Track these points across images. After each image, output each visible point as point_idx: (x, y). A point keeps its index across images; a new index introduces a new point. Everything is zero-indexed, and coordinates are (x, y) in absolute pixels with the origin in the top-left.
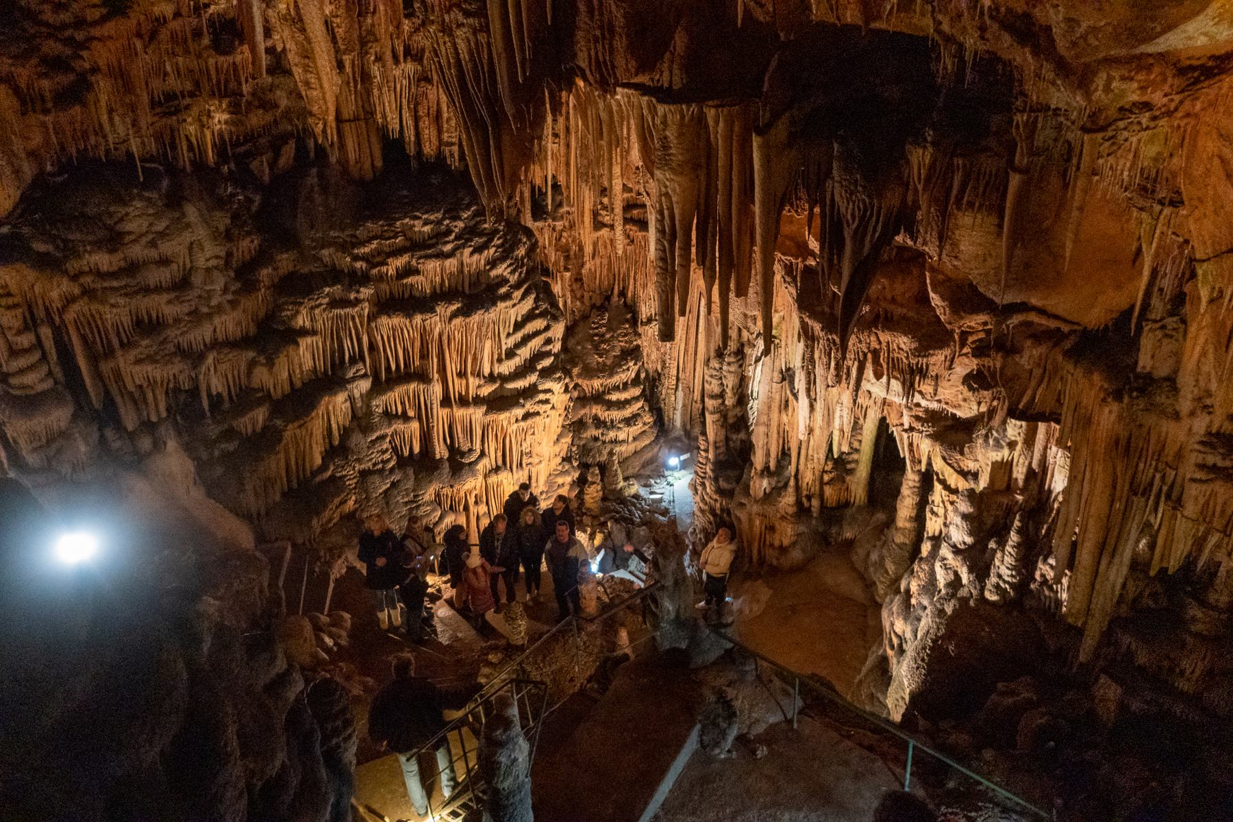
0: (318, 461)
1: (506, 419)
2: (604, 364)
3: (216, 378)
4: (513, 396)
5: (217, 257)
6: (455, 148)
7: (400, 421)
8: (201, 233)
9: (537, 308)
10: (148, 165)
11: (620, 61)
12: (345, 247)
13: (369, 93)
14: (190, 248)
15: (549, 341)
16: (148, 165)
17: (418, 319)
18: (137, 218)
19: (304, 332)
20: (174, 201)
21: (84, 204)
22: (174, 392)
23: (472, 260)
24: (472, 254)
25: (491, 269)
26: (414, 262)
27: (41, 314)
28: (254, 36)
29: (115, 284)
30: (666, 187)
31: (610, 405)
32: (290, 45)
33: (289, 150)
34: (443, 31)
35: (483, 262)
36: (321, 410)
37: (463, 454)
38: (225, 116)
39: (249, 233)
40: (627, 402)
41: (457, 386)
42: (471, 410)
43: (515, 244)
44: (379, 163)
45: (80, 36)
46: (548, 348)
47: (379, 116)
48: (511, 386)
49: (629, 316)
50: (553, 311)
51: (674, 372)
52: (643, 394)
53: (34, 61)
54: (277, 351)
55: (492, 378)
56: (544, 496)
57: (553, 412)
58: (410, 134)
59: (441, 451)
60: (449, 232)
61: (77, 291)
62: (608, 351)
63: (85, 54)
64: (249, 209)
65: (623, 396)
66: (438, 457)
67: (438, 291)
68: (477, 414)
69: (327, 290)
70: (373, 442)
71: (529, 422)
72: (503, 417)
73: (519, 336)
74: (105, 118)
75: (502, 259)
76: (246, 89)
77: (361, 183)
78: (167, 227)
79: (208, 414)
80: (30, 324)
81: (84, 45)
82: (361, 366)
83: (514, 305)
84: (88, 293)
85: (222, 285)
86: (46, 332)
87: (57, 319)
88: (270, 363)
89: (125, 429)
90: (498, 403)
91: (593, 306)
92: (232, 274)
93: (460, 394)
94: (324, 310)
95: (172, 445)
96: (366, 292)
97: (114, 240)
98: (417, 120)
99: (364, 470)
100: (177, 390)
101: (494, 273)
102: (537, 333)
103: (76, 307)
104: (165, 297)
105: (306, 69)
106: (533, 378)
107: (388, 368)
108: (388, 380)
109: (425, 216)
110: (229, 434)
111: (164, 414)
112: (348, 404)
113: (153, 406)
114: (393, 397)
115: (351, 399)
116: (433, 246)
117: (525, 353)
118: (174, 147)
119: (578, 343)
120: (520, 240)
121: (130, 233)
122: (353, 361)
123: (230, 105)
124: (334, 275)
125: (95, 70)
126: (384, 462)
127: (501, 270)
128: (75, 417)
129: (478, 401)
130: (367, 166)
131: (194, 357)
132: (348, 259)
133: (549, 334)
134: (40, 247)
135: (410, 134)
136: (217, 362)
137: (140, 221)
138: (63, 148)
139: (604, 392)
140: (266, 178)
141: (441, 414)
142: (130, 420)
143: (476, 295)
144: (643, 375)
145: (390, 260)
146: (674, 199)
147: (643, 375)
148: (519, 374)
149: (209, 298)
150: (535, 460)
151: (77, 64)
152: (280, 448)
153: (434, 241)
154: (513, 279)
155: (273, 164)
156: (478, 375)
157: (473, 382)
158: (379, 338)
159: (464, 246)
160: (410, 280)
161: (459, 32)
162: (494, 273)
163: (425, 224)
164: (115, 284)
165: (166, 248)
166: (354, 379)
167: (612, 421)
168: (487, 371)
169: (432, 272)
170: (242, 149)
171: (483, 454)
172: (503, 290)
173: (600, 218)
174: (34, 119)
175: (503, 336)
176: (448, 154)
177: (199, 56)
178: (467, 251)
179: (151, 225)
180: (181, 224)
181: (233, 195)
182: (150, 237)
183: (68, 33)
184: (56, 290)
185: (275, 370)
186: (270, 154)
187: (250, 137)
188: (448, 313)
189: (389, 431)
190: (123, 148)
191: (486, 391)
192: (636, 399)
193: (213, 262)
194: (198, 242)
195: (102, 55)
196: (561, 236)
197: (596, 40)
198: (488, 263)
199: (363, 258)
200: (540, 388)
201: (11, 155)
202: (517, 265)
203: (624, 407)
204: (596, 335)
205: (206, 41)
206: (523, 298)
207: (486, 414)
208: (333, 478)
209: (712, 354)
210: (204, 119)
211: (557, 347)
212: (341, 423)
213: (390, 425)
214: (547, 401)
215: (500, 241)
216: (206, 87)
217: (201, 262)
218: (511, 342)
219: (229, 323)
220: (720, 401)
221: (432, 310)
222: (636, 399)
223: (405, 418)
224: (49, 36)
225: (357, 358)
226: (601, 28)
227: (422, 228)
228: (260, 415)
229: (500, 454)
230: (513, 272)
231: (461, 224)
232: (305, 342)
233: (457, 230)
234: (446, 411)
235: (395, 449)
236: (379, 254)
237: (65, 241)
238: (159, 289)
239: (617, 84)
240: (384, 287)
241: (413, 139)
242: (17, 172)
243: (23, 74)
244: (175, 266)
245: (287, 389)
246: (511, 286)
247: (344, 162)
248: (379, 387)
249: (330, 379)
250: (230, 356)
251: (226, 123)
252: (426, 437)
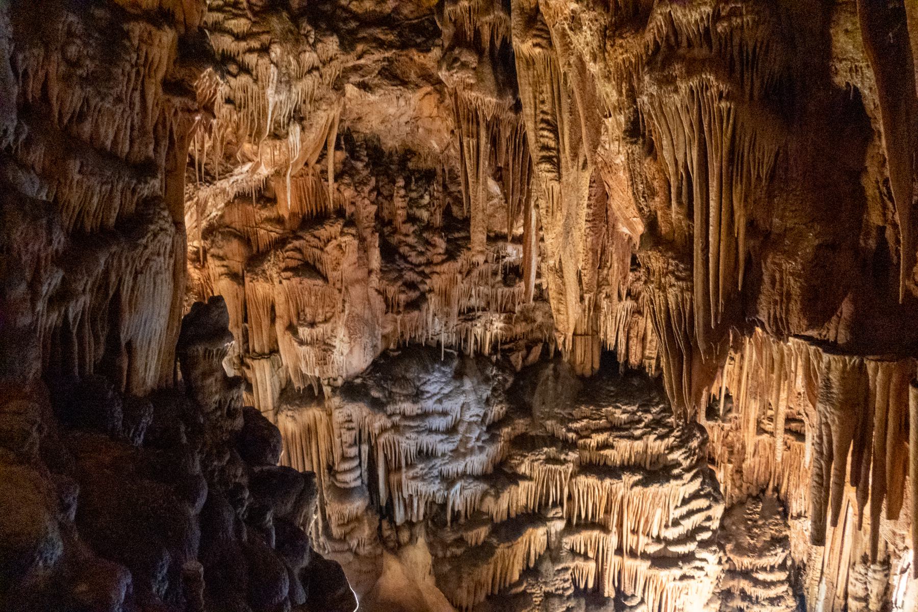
0: (516, 577)
1: (666, 576)
2: (755, 546)
3: (460, 497)
4: (673, 558)
5: (478, 415)
6: (653, 362)
7: (582, 559)
8: (472, 398)
9: (702, 490)
10: (448, 350)
11: (794, 320)
12: (563, 421)
13: (597, 318)
14: (462, 407)
15: (709, 519)
16: (448, 350)
17: (607, 482)
18: (435, 383)
19: (524, 477)
20: (459, 375)
21: (407, 371)
22: (431, 504)
23: (655, 445)
24: (655, 440)
25: (669, 453)
26: (611, 440)
27: (365, 436)
28: (529, 278)
29: (412, 424)
30: (826, 418)
31: (756, 582)
32: (552, 286)
33: (537, 351)
34: (659, 289)
35: (663, 447)
36: (525, 538)
37: (626, 598)
38: (501, 325)
39: (501, 402)
40: (772, 584)
41: (630, 541)
43: (691, 437)
44: (597, 366)
45: (427, 271)
46: (707, 524)
47: (602, 334)
48: (673, 549)
49: (781, 509)
50: (715, 494)
51: (820, 567)
52: (788, 579)
53: (400, 283)
54: (503, 488)
55: (658, 540)
58: (622, 349)
59: (609, 591)
60: (640, 421)
61: (389, 425)
62: (759, 535)
63: (428, 281)
64: (504, 386)
65: (769, 577)
66: (606, 595)
67: (626, 463)
68: (643, 566)
69: (545, 449)
70: (559, 571)
71: (685, 582)
73: (684, 510)
74: (430, 319)
75: (679, 447)
76: (518, 309)
77: (582, 378)
78: (451, 392)
79: (449, 524)
80: (358, 442)
81: (427, 276)
82: (559, 510)
83: (684, 485)
84: (395, 427)
85: (477, 435)
86: (365, 448)
87: (373, 442)
88: (497, 497)
89: (395, 523)
90: (661, 561)
91: (749, 495)
92: (485, 429)
93: (631, 547)
94: (541, 464)
95: (421, 541)
96: (573, 456)
97: (417, 396)
98: (628, 339)
99: (548, 592)
100: (433, 502)
101: (670, 457)
102: (700, 510)
103: (386, 435)
104: (440, 437)
105: (559, 301)
106: (691, 547)
107: (579, 516)
108: (577, 525)
109: (624, 407)
110: (460, 541)
111: (421, 518)
112: (545, 537)
113: (415, 511)
114: (579, 539)
115: (548, 534)
116: (627, 430)
117: (688, 525)
118: (466, 340)
119: (733, 524)
120: (695, 435)
121: (428, 392)
122: (555, 505)
123: (505, 318)
124: (552, 440)
125: (431, 291)
126: (565, 589)
127: (677, 455)
128: (368, 508)
129: (645, 556)
130: (588, 367)
131: (449, 481)
132: (564, 430)
133: (710, 513)
134: (375, 394)
135: (622, 349)
136: (463, 488)
137: (435, 385)
138: (402, 335)
139: (752, 570)
140: (519, 368)
141: (613, 561)
142: (400, 516)
143: (655, 472)
144: (789, 563)
145: (593, 435)
146: (833, 428)
147: (789, 563)
149: (467, 443)
151: (421, 287)
152: (492, 560)
153: (628, 426)
154: (686, 464)
155: (525, 359)
156: (648, 535)
157: (643, 540)
158: (576, 492)
159: (650, 433)
161: (670, 290)
162: (670, 457)
163: (623, 413)
164: (412, 424)
165: (447, 405)
166: (553, 519)
167: (757, 598)
168: (655, 534)
169: (622, 449)
170: (507, 347)
171: (642, 601)
173: (762, 426)
174: (390, 315)
175: (672, 507)
176: (647, 365)
177: (493, 287)
178: (652, 437)
179: (442, 388)
180: (458, 391)
181: (496, 376)
182: (439, 396)
183: (421, 269)
184: (379, 421)
185: (499, 501)
186: (524, 352)
187: (514, 340)
188: (631, 482)
190: (436, 338)
191: (653, 549)
192: (782, 582)
193: (474, 419)
194: (463, 403)
195: (437, 282)
196: (728, 435)
197: (776, 302)
198: (667, 448)
199: (576, 431)
200: (698, 556)
201: (373, 335)
202: (691, 453)
203: (769, 587)
204: (750, 520)
205: (499, 278)
206: (692, 480)
207: (650, 567)
208: (524, 592)
209: (858, 559)
210: (488, 325)
211: (715, 525)
212: (538, 550)
213: (573, 560)
214: (702, 569)
215: (679, 433)
216: (493, 306)
217: (467, 418)
218: (677, 514)
219: (477, 462)
220: (864, 604)
221: (619, 478)
222: (782, 582)
223: (586, 557)
224: (411, 269)
225: (558, 504)
226: (781, 295)
227: (620, 415)
228: (483, 532)
229: (657, 604)
230: (686, 458)
231: (650, 417)
232: (523, 484)
233: (646, 420)
235: (574, 581)
236: (586, 429)
237: (390, 393)
238: (437, 431)
239: (789, 335)
240: (586, 454)
241: (623, 352)
242: (375, 346)
243: (392, 290)
244: (449, 418)
245: (505, 517)
246: (683, 469)
247: (572, 363)
248: (570, 528)
249: (534, 516)
250: (472, 485)
251: (501, 329)
252: (599, 577)
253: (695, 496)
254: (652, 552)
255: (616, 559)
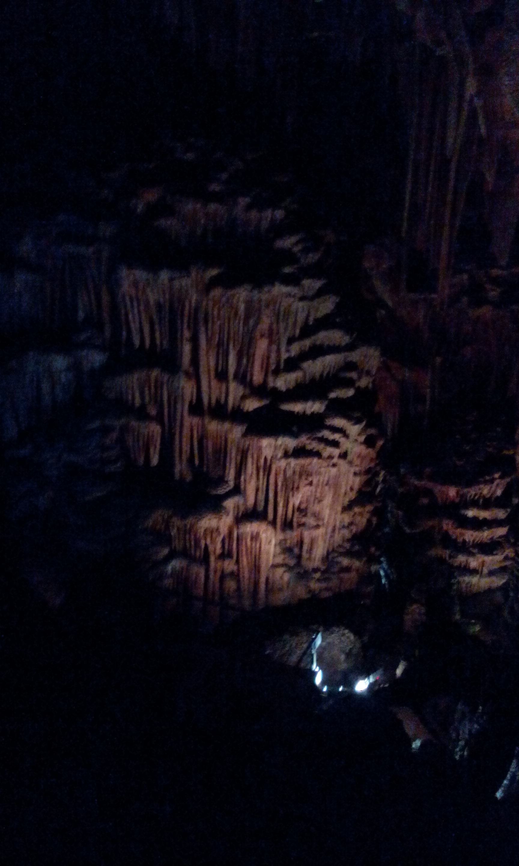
24: (249, 208)
41: (211, 390)
42: (227, 425)
55: (260, 391)
56: (318, 575)
57: (341, 462)
65: (484, 514)
72: (268, 446)
73: (307, 343)
96: (107, 230)
106: (315, 407)
129: (237, 415)
143: (248, 262)
148: (300, 392)
150: (311, 521)
157: (235, 390)
160: (164, 223)
169: (195, 213)
172: (287, 270)
178: (243, 201)
189: (118, 423)
191: (252, 405)
214: (335, 444)
218: (295, 349)
234: (196, 420)
253: (325, 323)
254: (251, 409)
255: (190, 421)
